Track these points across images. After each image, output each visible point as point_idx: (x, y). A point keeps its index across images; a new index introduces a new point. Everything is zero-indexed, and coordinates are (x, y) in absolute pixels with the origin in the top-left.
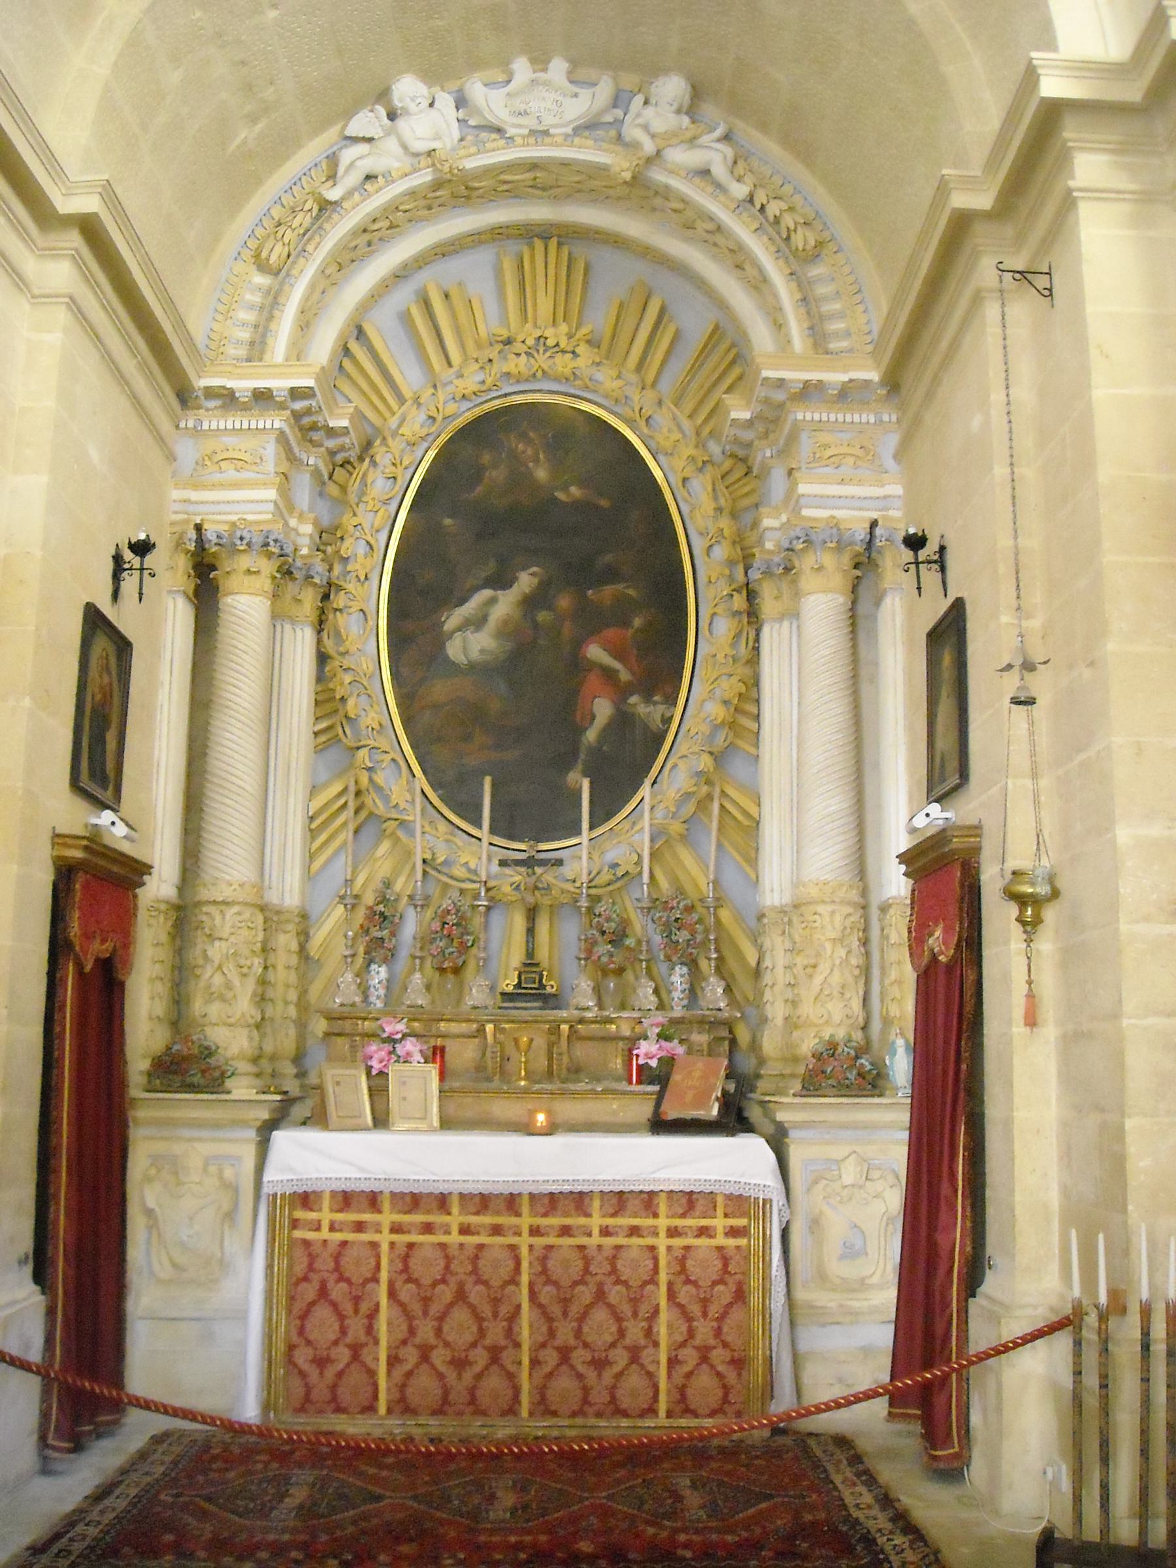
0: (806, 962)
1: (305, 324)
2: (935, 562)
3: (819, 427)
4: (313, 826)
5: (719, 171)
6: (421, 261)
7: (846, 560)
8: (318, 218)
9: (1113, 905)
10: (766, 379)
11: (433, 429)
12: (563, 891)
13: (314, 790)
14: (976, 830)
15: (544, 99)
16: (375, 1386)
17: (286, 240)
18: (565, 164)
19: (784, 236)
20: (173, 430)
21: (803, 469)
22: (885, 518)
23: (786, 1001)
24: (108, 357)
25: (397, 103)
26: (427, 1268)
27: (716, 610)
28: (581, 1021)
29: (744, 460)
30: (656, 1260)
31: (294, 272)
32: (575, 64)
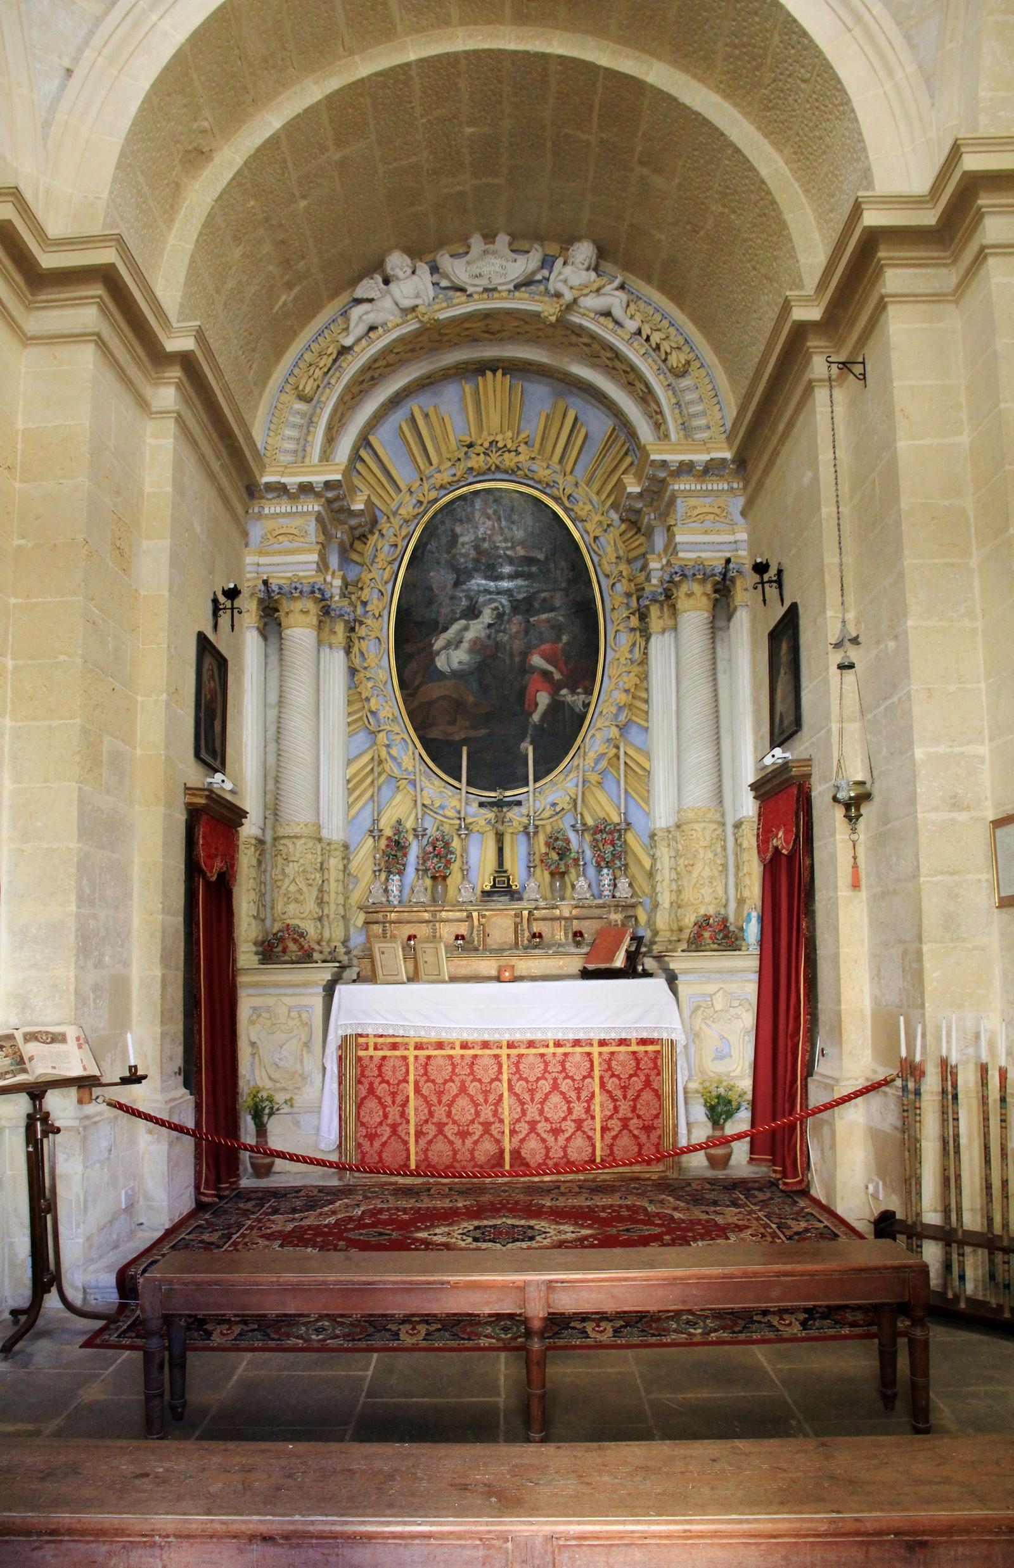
1: (331, 439)
3: (690, 494)
4: (350, 786)
5: (618, 312)
7: (709, 588)
8: (335, 361)
9: (913, 800)
10: (653, 461)
11: (422, 509)
13: (349, 762)
14: (808, 762)
16: (408, 1150)
17: (316, 376)
18: (509, 313)
19: (663, 357)
22: (736, 557)
25: (390, 272)
28: (536, 909)
30: (592, 1062)
32: (514, 237)
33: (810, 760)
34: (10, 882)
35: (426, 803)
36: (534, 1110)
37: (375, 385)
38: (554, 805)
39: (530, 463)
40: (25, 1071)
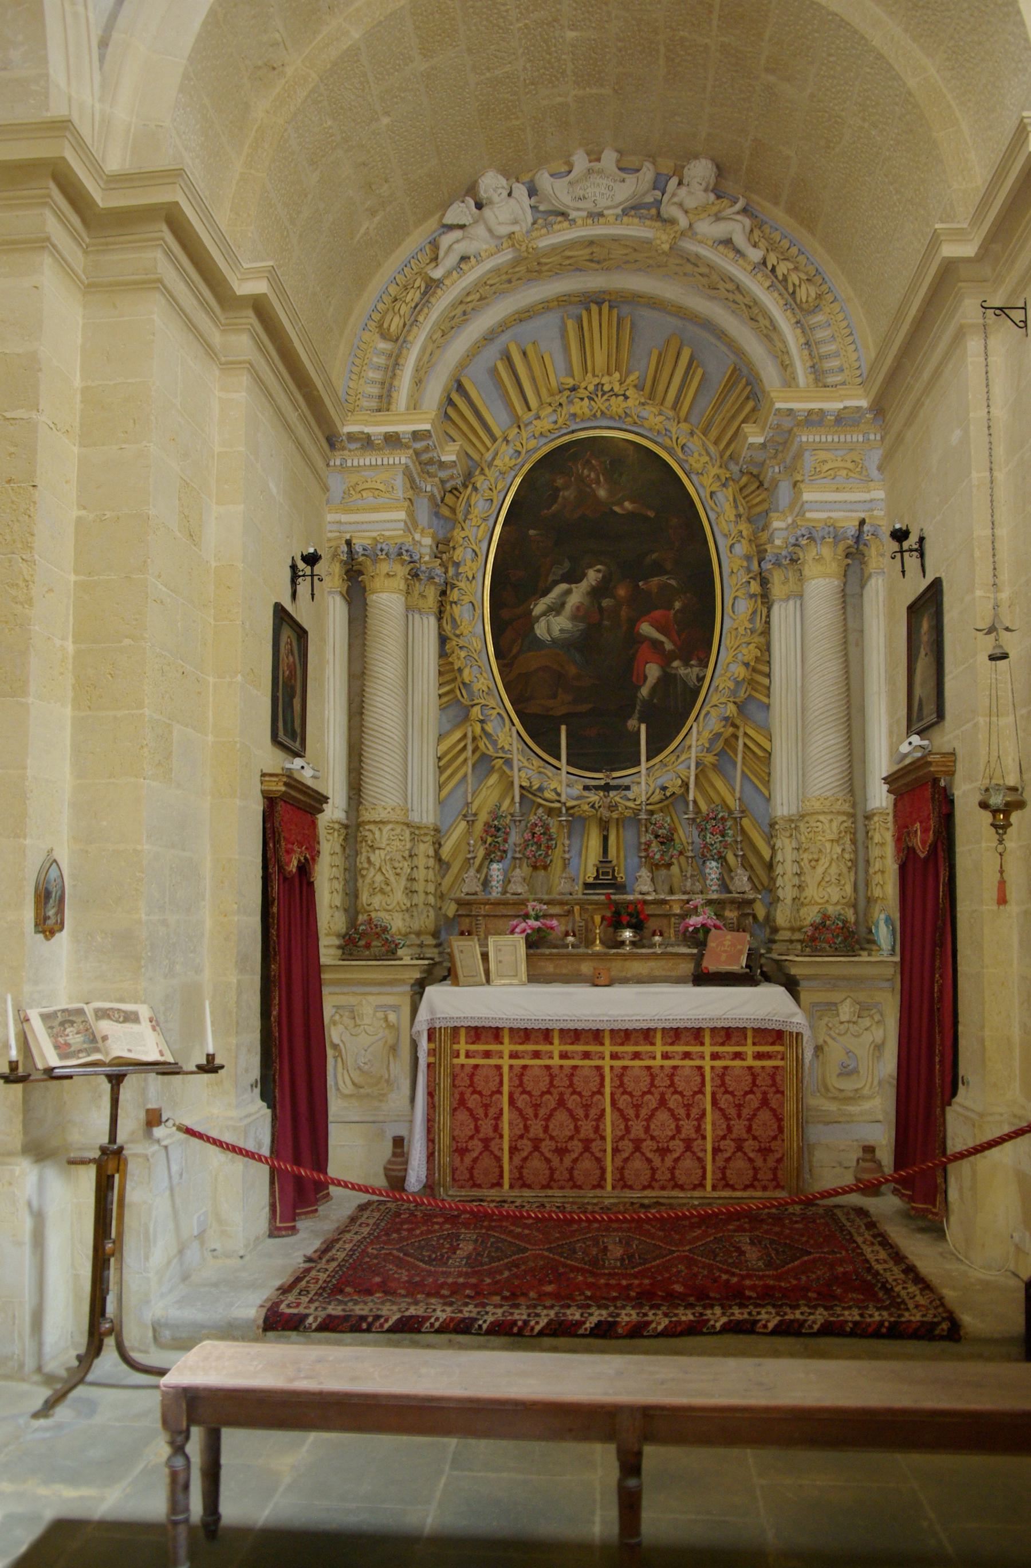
0: (810, 857)
2: (916, 550)
4: (441, 764)
5: (740, 240)
6: (504, 326)
8: (425, 293)
10: (778, 410)
12: (627, 808)
13: (441, 738)
15: (598, 185)
16: (501, 1167)
17: (402, 312)
18: (615, 239)
19: (791, 290)
20: (324, 467)
21: (807, 481)
23: (794, 886)
24: (278, 411)
25: (483, 194)
26: (536, 1084)
27: (737, 594)
29: (756, 477)
30: (703, 1076)
31: (410, 338)
33: (953, 754)
34: (74, 886)
35: (524, 784)
36: (640, 1128)
37: (466, 320)
38: (664, 788)
39: (640, 409)
40: (97, 1050)
